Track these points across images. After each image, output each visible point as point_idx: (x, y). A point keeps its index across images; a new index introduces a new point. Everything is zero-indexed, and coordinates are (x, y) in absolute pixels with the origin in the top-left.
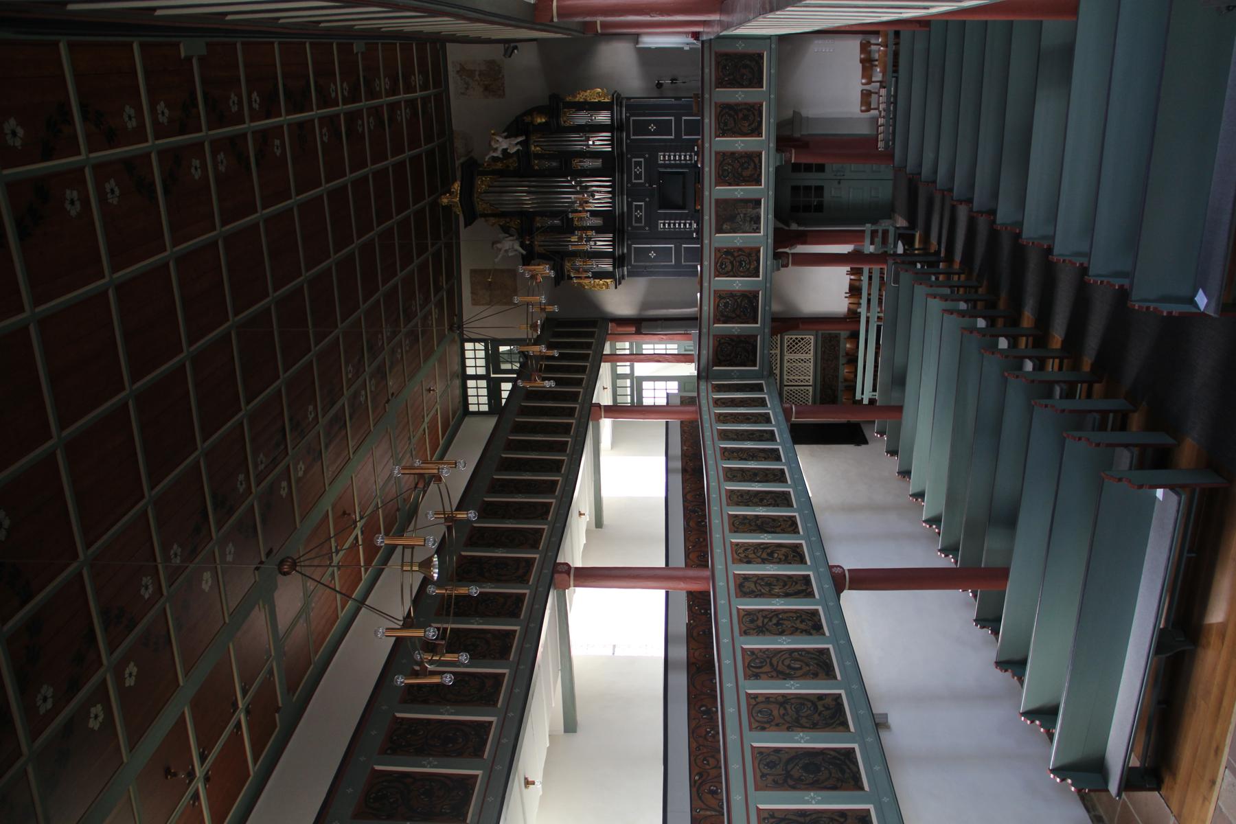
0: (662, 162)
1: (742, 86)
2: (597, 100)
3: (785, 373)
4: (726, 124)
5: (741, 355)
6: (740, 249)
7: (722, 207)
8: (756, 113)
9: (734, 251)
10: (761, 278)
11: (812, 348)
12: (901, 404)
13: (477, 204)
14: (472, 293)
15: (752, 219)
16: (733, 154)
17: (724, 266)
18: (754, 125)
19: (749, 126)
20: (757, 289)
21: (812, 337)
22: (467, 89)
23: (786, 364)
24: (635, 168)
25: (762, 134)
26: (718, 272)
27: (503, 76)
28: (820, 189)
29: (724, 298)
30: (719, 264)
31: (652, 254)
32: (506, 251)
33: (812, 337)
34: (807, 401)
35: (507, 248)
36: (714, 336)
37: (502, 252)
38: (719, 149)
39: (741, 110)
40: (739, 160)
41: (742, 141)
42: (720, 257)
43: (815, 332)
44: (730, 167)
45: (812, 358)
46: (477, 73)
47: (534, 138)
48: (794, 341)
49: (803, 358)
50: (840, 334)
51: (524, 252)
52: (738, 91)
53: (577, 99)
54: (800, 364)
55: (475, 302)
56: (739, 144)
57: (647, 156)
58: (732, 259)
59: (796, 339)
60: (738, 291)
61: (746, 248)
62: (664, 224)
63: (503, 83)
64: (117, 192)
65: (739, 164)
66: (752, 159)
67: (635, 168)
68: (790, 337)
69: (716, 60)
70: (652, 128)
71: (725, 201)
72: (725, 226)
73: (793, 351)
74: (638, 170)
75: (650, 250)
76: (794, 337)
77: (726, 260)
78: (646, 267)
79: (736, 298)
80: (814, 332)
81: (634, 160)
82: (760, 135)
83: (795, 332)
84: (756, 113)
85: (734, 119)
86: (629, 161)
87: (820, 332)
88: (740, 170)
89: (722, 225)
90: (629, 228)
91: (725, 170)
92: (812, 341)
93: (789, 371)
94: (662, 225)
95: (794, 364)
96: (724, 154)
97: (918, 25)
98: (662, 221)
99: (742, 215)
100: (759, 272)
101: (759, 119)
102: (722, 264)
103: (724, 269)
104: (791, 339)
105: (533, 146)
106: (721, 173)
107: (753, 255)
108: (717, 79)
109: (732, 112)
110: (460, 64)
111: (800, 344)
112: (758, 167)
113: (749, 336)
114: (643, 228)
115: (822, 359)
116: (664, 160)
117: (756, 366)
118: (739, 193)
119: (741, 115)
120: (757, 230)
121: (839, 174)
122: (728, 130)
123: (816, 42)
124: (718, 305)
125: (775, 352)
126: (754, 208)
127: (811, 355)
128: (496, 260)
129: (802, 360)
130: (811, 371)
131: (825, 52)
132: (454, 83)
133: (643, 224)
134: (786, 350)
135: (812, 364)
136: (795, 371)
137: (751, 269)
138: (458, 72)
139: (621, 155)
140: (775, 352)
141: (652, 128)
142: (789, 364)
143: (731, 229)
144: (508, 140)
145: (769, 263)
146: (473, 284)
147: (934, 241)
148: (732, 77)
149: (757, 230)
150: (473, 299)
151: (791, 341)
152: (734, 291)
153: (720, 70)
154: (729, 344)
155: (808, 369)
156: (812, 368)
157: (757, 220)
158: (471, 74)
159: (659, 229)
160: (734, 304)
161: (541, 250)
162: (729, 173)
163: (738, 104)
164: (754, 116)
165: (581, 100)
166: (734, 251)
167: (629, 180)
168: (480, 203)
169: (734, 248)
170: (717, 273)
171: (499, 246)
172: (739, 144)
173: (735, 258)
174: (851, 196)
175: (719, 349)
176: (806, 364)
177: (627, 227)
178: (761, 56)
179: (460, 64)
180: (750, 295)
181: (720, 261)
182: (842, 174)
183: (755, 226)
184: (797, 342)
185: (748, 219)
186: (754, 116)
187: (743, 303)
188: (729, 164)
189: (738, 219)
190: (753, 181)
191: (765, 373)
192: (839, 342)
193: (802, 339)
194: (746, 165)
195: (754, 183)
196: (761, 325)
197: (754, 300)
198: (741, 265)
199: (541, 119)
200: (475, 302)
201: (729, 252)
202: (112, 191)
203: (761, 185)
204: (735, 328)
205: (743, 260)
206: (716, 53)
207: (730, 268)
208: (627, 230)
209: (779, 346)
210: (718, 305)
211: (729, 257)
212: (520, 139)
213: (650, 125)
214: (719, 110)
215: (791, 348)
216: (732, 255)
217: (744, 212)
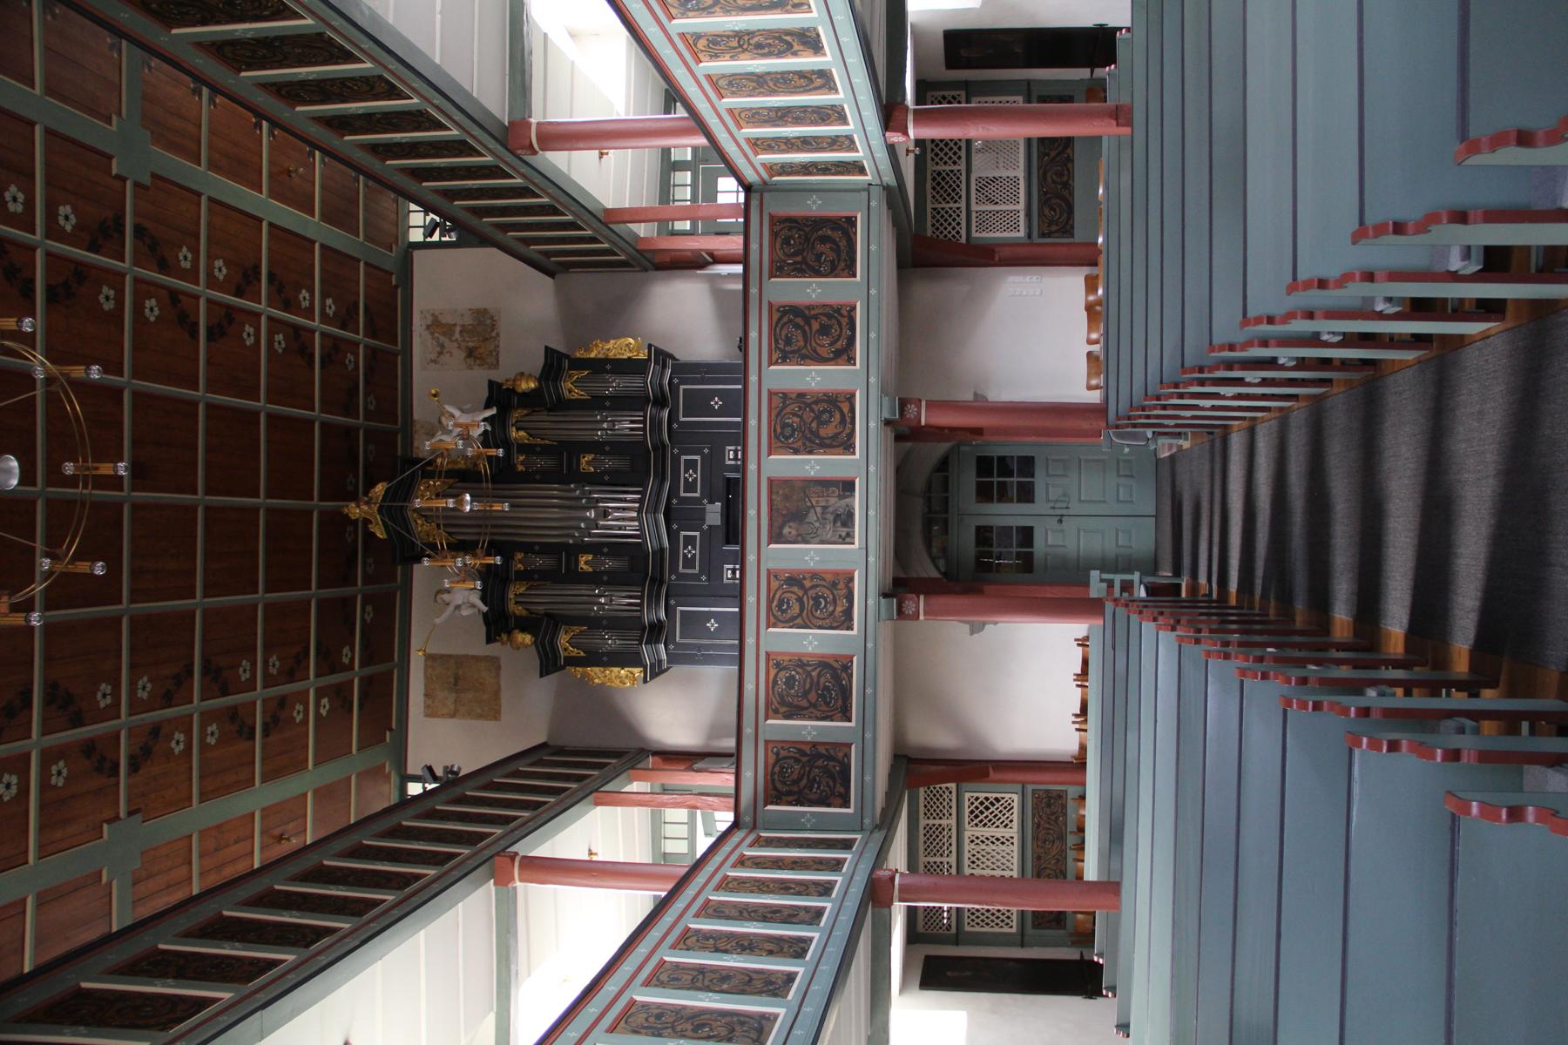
0: (733, 462)
1: (818, 274)
2: (625, 357)
3: (967, 862)
4: (788, 341)
5: (819, 784)
6: (815, 575)
7: (781, 492)
8: (844, 321)
9: (804, 578)
10: (855, 632)
11: (1015, 817)
12: (1117, 880)
13: (413, 524)
14: (426, 695)
15: (837, 517)
16: (801, 395)
18: (839, 343)
19: (830, 345)
20: (851, 653)
21: (1015, 797)
22: (440, 353)
23: (967, 847)
24: (686, 472)
25: (855, 360)
26: (774, 616)
27: (498, 334)
28: (1027, 534)
29: (785, 668)
30: (775, 603)
31: (712, 625)
32: (458, 607)
33: (1015, 797)
34: (1008, 917)
35: (460, 602)
36: (767, 742)
37: (451, 608)
38: (776, 386)
39: (816, 317)
40: (813, 406)
43: (1020, 786)
44: (797, 420)
45: (1016, 836)
46: (458, 329)
47: (516, 415)
48: (982, 803)
49: (998, 835)
50: (1066, 791)
51: (485, 609)
52: (811, 283)
53: (592, 355)
54: (994, 847)
55: (431, 712)
56: (814, 377)
59: (987, 799)
60: (811, 655)
61: (826, 572)
64: (327, 707)
66: (837, 405)
68: (975, 795)
69: (771, 230)
70: (716, 403)
71: (787, 483)
72: (786, 530)
73: (981, 821)
74: (691, 475)
75: (709, 615)
76: (982, 796)
78: (699, 647)
79: (809, 669)
82: (851, 360)
83: (981, 786)
84: (844, 321)
85: (804, 333)
86: (676, 460)
87: (1030, 788)
88: (814, 425)
89: (781, 528)
90: (673, 577)
92: (1015, 805)
94: (730, 572)
95: (983, 846)
97: (1114, 123)
98: (731, 566)
99: (819, 510)
100: (851, 619)
101: (849, 333)
102: (781, 602)
103: (784, 611)
104: (977, 799)
105: (514, 429)
107: (841, 585)
108: (771, 262)
109: (799, 320)
112: (848, 420)
113: (836, 745)
114: (696, 577)
115: (1035, 838)
118: (812, 468)
119: (815, 326)
120: (847, 538)
121: (1058, 505)
122: (793, 352)
123: (1011, 279)
124: (775, 682)
125: (948, 822)
126: (841, 497)
127: (1014, 831)
128: (438, 621)
129: (998, 839)
130: (1015, 861)
131: (1027, 295)
132: (421, 343)
133: (696, 571)
134: (967, 820)
135: (1015, 848)
136: (984, 860)
137: (836, 613)
140: (948, 822)
141: (716, 403)
142: (972, 846)
145: (871, 602)
147: (1203, 580)
148: (799, 259)
149: (847, 538)
150: (427, 707)
151: (976, 804)
154: (797, 760)
155: (1009, 857)
156: (1015, 854)
157: (847, 519)
158: (448, 330)
159: (725, 581)
160: (805, 681)
161: (519, 610)
163: (810, 307)
166: (804, 578)
171: (446, 597)
172: (814, 377)
173: (806, 591)
174: (1081, 544)
175: (777, 769)
176: (1003, 847)
178: (851, 221)
179: (433, 315)
180: (835, 665)
181: (777, 596)
182: (1065, 505)
183: (843, 532)
184: (987, 804)
185: (831, 517)
188: (795, 415)
189: (812, 517)
190: (838, 446)
191: (867, 821)
192: (1064, 806)
193: (997, 800)
194: (825, 416)
197: (844, 675)
198: (817, 604)
199: (527, 383)
200: (431, 712)
201: (794, 580)
202: (245, 671)
204: (808, 728)
205: (825, 599)
206: (772, 217)
207: (796, 610)
209: (954, 811)
210: (775, 682)
211: (795, 589)
213: (713, 399)
214: (776, 316)
215: (977, 817)
216: (802, 586)
217: (823, 504)
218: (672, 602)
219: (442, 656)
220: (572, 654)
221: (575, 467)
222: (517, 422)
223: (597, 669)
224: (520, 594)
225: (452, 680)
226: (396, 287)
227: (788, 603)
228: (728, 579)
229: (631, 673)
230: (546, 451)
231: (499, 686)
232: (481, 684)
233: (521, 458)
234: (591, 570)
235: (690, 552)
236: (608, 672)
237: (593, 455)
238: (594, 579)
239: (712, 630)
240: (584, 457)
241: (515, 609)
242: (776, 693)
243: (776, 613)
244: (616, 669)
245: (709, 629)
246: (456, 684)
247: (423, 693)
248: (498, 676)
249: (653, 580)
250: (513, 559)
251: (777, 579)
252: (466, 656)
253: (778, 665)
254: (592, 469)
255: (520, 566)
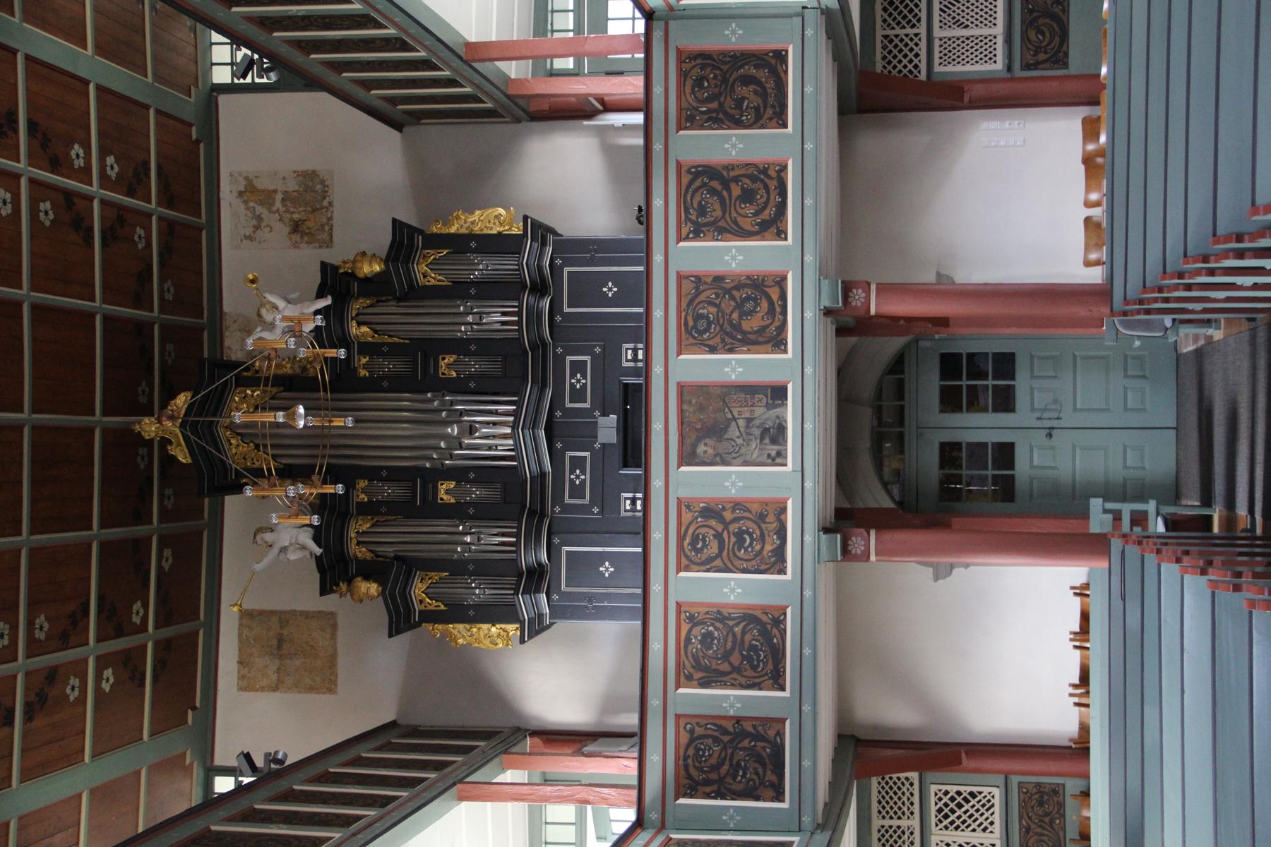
0: (631, 364)
1: (739, 124)
2: (494, 232)
4: (702, 211)
6: (737, 505)
8: (772, 184)
9: (724, 509)
11: (997, 818)
13: (226, 445)
15: (765, 431)
16: (719, 279)
17: (699, 546)
18: (766, 212)
19: (756, 214)
20: (783, 603)
21: (996, 791)
22: (257, 228)
24: (573, 376)
27: (330, 204)
28: (1005, 453)
31: (607, 569)
32: (284, 550)
35: (287, 544)
37: (275, 550)
39: (736, 180)
41: (738, 249)
42: (692, 522)
44: (713, 310)
46: (279, 197)
47: (357, 306)
48: (953, 799)
51: (318, 551)
52: (731, 136)
53: (453, 230)
57: (598, 350)
58: (720, 528)
60: (734, 606)
61: (752, 501)
62: (633, 501)
63: (330, 219)
65: (733, 303)
67: (573, 376)
68: (944, 788)
72: (701, 449)
73: (952, 823)
74: (578, 381)
75: (602, 557)
77: (706, 530)
78: (590, 598)
79: (731, 623)
80: (1000, 779)
81: (569, 358)
84: (772, 184)
86: (560, 361)
88: (735, 316)
89: (695, 446)
91: (701, 316)
92: (997, 801)
93: (891, 832)
96: (698, 279)
98: (630, 495)
99: (741, 423)
102: (695, 539)
103: (698, 551)
104: (946, 793)
105: (354, 323)
106: (691, 323)
107: (771, 518)
108: (680, 110)
110: (246, 178)
111: (966, 807)
112: (778, 310)
114: (586, 509)
116: (635, 359)
117: (783, 801)
118: (733, 370)
119: (736, 191)
120: (778, 458)
121: (1045, 415)
122: (706, 225)
123: (985, 125)
124: (688, 640)
126: (769, 407)
133: (586, 501)
134: (934, 820)
137: (765, 553)
138: (241, 194)
139: (540, 346)
141: (610, 289)
143: (716, 455)
144: (299, 305)
146: (243, 643)
148: (714, 105)
150: (242, 677)
151: (946, 799)
152: (727, 605)
153: (688, 90)
154: (716, 740)
157: (776, 434)
158: (266, 198)
159: (623, 513)
161: (362, 553)
162: (710, 323)
163: (729, 167)
164: (768, 192)
165: (463, 231)
166: (724, 509)
167: (556, 403)
168: (233, 441)
169: (723, 501)
170: (684, 560)
171: (268, 537)
173: (726, 525)
175: (691, 752)
177: (553, 507)
178: (781, 56)
180: (764, 618)
181: (690, 532)
182: (1055, 415)
183: (773, 449)
185: (757, 432)
186: (768, 192)
187: (748, 637)
188: (711, 303)
189: (733, 432)
191: (806, 819)
192: (1061, 805)
193: (973, 795)
194: (749, 306)
195: (769, 347)
196: (791, 693)
197: (775, 631)
198: (741, 541)
199: (370, 265)
200: (246, 685)
201: (711, 511)
203: (785, 351)
206: (679, 52)
207: (714, 548)
208: (553, 512)
209: (916, 808)
210: (688, 640)
211: (713, 523)
212: (322, 304)
214: (686, 179)
215: (946, 817)
216: (721, 519)
217: (747, 415)
218: (556, 541)
219: (262, 613)
220: (430, 608)
221: (431, 498)
222: (358, 315)
223: (461, 627)
224: (363, 532)
225: (275, 642)
226: (198, 142)
227: (704, 540)
228: (626, 511)
229: (504, 630)
230: (395, 351)
231: (335, 650)
232: (313, 647)
233: (364, 360)
234: (453, 501)
235: (578, 477)
236: (474, 630)
237: (455, 357)
238: (457, 512)
239: (607, 575)
240: (444, 359)
241: (357, 551)
242: (689, 654)
243: (689, 553)
244: (485, 626)
245: (602, 574)
246: (279, 647)
247: (236, 659)
248: (334, 635)
249: (532, 513)
250: (354, 488)
251: (690, 510)
252: (293, 612)
253: (691, 618)
254: (454, 374)
255: (363, 496)
